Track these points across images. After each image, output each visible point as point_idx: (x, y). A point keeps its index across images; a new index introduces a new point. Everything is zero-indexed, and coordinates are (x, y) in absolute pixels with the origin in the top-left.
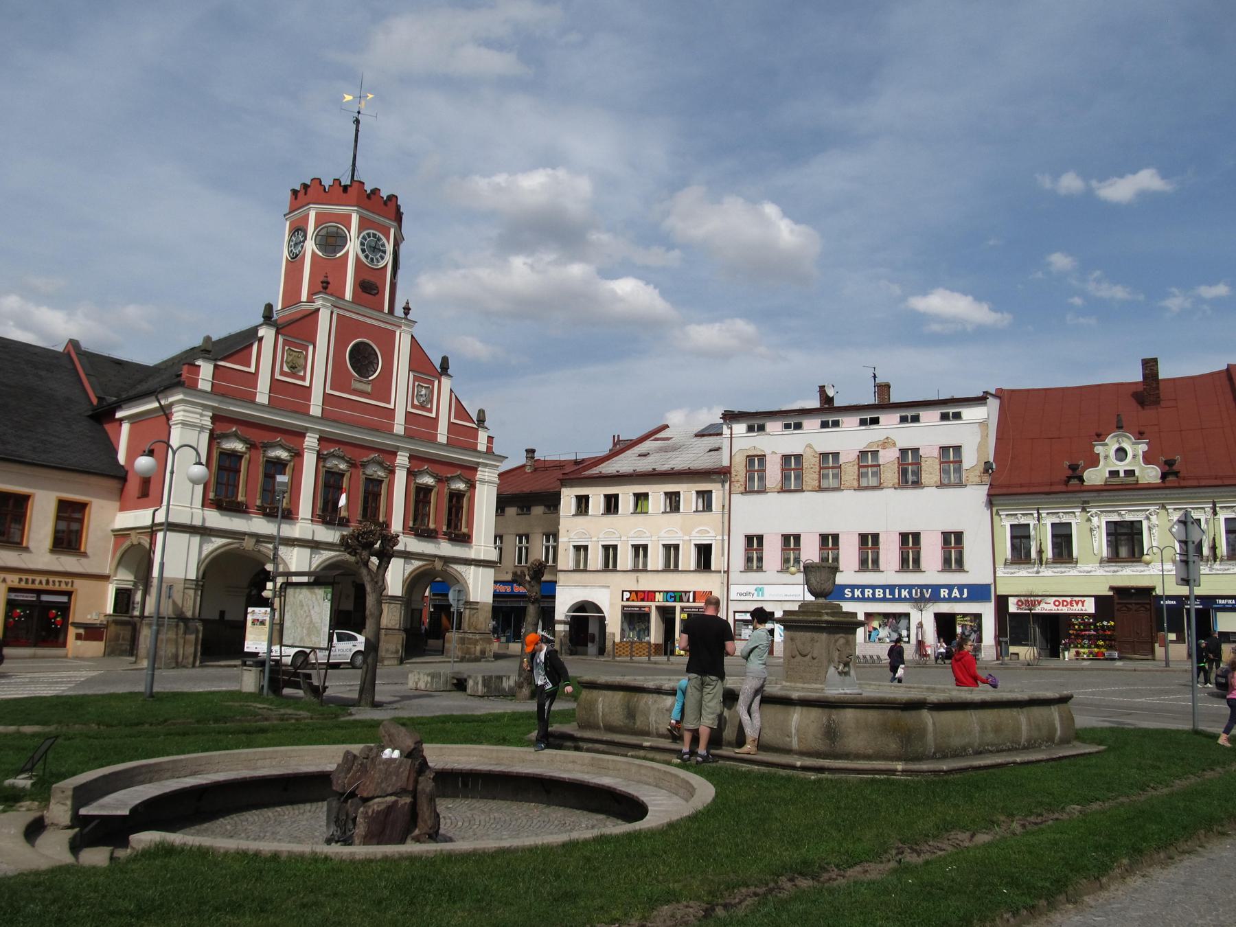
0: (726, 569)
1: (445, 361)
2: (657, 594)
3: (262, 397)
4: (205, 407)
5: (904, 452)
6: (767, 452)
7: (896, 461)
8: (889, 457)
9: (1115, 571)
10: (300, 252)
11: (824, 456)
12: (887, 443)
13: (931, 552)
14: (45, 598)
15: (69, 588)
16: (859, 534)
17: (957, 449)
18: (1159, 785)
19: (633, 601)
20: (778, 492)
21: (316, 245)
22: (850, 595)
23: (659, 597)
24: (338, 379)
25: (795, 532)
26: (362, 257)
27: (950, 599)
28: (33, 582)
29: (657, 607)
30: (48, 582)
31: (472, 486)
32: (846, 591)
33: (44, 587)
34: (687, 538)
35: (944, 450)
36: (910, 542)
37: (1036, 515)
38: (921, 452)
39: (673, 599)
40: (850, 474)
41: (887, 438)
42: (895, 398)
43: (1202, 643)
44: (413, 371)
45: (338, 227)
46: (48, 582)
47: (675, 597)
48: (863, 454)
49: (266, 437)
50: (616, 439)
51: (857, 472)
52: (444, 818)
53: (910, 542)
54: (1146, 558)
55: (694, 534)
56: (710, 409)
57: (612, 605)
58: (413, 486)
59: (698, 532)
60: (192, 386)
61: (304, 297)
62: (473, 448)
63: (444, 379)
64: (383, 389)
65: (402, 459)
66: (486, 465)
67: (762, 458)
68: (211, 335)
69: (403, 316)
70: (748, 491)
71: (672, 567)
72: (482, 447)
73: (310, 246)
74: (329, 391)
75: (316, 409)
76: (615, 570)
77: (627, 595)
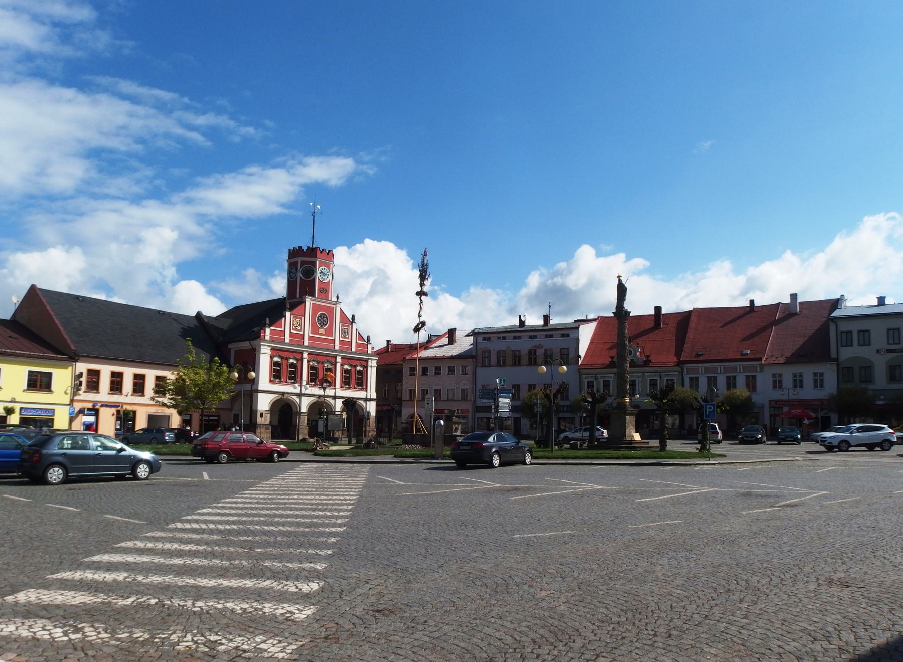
1: (353, 317)
4: (268, 346)
5: (546, 350)
12: (540, 346)
14: (211, 418)
15: (218, 414)
23: (446, 412)
24: (314, 330)
26: (320, 278)
27: (564, 412)
29: (445, 416)
30: (798, 382)
46: (798, 382)
48: (530, 352)
49: (324, 359)
55: (461, 384)
56: (629, 258)
61: (298, 296)
62: (367, 354)
63: (354, 325)
64: (330, 332)
65: (339, 359)
70: (483, 365)
73: (300, 275)
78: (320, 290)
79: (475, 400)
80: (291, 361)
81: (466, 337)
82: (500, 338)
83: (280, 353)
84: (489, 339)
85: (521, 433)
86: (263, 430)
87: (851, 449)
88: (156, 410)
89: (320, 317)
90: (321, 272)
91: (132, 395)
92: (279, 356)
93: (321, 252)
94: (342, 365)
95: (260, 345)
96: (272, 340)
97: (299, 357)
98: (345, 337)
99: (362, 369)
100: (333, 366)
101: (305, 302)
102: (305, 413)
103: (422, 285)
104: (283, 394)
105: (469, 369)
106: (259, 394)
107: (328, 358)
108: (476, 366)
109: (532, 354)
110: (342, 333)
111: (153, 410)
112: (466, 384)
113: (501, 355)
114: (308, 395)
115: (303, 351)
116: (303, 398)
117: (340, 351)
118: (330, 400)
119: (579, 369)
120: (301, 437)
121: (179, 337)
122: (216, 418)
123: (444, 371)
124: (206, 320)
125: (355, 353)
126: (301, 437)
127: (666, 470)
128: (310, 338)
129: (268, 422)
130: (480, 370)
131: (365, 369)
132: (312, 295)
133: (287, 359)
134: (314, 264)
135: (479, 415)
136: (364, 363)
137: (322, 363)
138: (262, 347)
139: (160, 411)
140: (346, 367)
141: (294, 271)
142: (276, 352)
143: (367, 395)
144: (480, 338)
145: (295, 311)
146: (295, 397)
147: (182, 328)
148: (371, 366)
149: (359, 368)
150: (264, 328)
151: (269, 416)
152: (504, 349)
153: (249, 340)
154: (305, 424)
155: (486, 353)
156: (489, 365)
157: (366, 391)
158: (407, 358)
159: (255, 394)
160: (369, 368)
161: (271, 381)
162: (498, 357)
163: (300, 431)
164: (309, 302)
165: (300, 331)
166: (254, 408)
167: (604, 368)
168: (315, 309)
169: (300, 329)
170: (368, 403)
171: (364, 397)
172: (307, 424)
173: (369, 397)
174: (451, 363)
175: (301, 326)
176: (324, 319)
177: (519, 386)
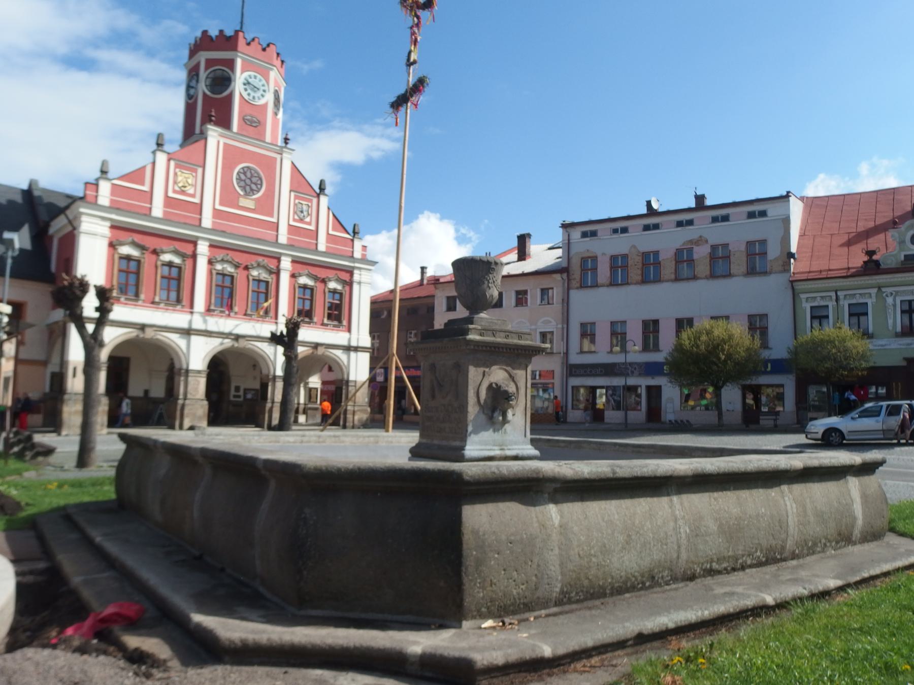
0: (565, 351)
3: (158, 210)
5: (714, 248)
6: (599, 254)
7: (708, 256)
8: (701, 253)
9: (908, 344)
11: (645, 255)
12: (700, 241)
16: (676, 319)
17: (763, 242)
20: (608, 286)
21: (206, 86)
24: (228, 196)
31: (349, 284)
32: (665, 368)
34: (533, 327)
35: (750, 244)
36: (651, 328)
37: (834, 298)
38: (730, 248)
40: (668, 270)
41: (701, 237)
42: (709, 202)
43: (882, 389)
45: (223, 70)
48: (679, 252)
49: (252, 260)
51: (674, 267)
52: (359, 283)
55: (539, 324)
58: (116, 257)
59: (542, 322)
60: (94, 204)
64: (267, 205)
65: (286, 264)
66: (360, 269)
67: (594, 259)
68: (493, 434)
69: (284, 145)
70: (583, 286)
74: (218, 207)
75: (207, 221)
78: (243, 119)
79: (567, 354)
82: (615, 231)
83: (138, 238)
84: (594, 234)
85: (663, 419)
87: (313, 345)
90: (247, 83)
92: (310, 276)
94: (293, 276)
96: (115, 207)
98: (301, 220)
100: (274, 276)
102: (199, 372)
104: (143, 327)
105: (556, 294)
107: (260, 259)
108: (568, 289)
109: (684, 258)
110: (295, 213)
112: (549, 320)
113: (618, 263)
116: (194, 338)
117: (290, 246)
118: (339, 353)
119: (792, 282)
128: (217, 214)
130: (578, 297)
132: (224, 122)
134: (231, 64)
135: (574, 381)
136: (345, 277)
137: (246, 268)
140: (303, 280)
143: (349, 340)
144: (576, 234)
148: (359, 283)
149: (332, 285)
152: (625, 251)
155: (589, 264)
156: (595, 285)
157: (349, 330)
160: (356, 287)
162: (613, 268)
163: (186, 411)
165: (193, 196)
166: (65, 359)
167: (853, 276)
168: (230, 156)
170: (353, 354)
171: (345, 343)
173: (354, 344)
175: (195, 186)
176: (254, 180)
177: (656, 322)
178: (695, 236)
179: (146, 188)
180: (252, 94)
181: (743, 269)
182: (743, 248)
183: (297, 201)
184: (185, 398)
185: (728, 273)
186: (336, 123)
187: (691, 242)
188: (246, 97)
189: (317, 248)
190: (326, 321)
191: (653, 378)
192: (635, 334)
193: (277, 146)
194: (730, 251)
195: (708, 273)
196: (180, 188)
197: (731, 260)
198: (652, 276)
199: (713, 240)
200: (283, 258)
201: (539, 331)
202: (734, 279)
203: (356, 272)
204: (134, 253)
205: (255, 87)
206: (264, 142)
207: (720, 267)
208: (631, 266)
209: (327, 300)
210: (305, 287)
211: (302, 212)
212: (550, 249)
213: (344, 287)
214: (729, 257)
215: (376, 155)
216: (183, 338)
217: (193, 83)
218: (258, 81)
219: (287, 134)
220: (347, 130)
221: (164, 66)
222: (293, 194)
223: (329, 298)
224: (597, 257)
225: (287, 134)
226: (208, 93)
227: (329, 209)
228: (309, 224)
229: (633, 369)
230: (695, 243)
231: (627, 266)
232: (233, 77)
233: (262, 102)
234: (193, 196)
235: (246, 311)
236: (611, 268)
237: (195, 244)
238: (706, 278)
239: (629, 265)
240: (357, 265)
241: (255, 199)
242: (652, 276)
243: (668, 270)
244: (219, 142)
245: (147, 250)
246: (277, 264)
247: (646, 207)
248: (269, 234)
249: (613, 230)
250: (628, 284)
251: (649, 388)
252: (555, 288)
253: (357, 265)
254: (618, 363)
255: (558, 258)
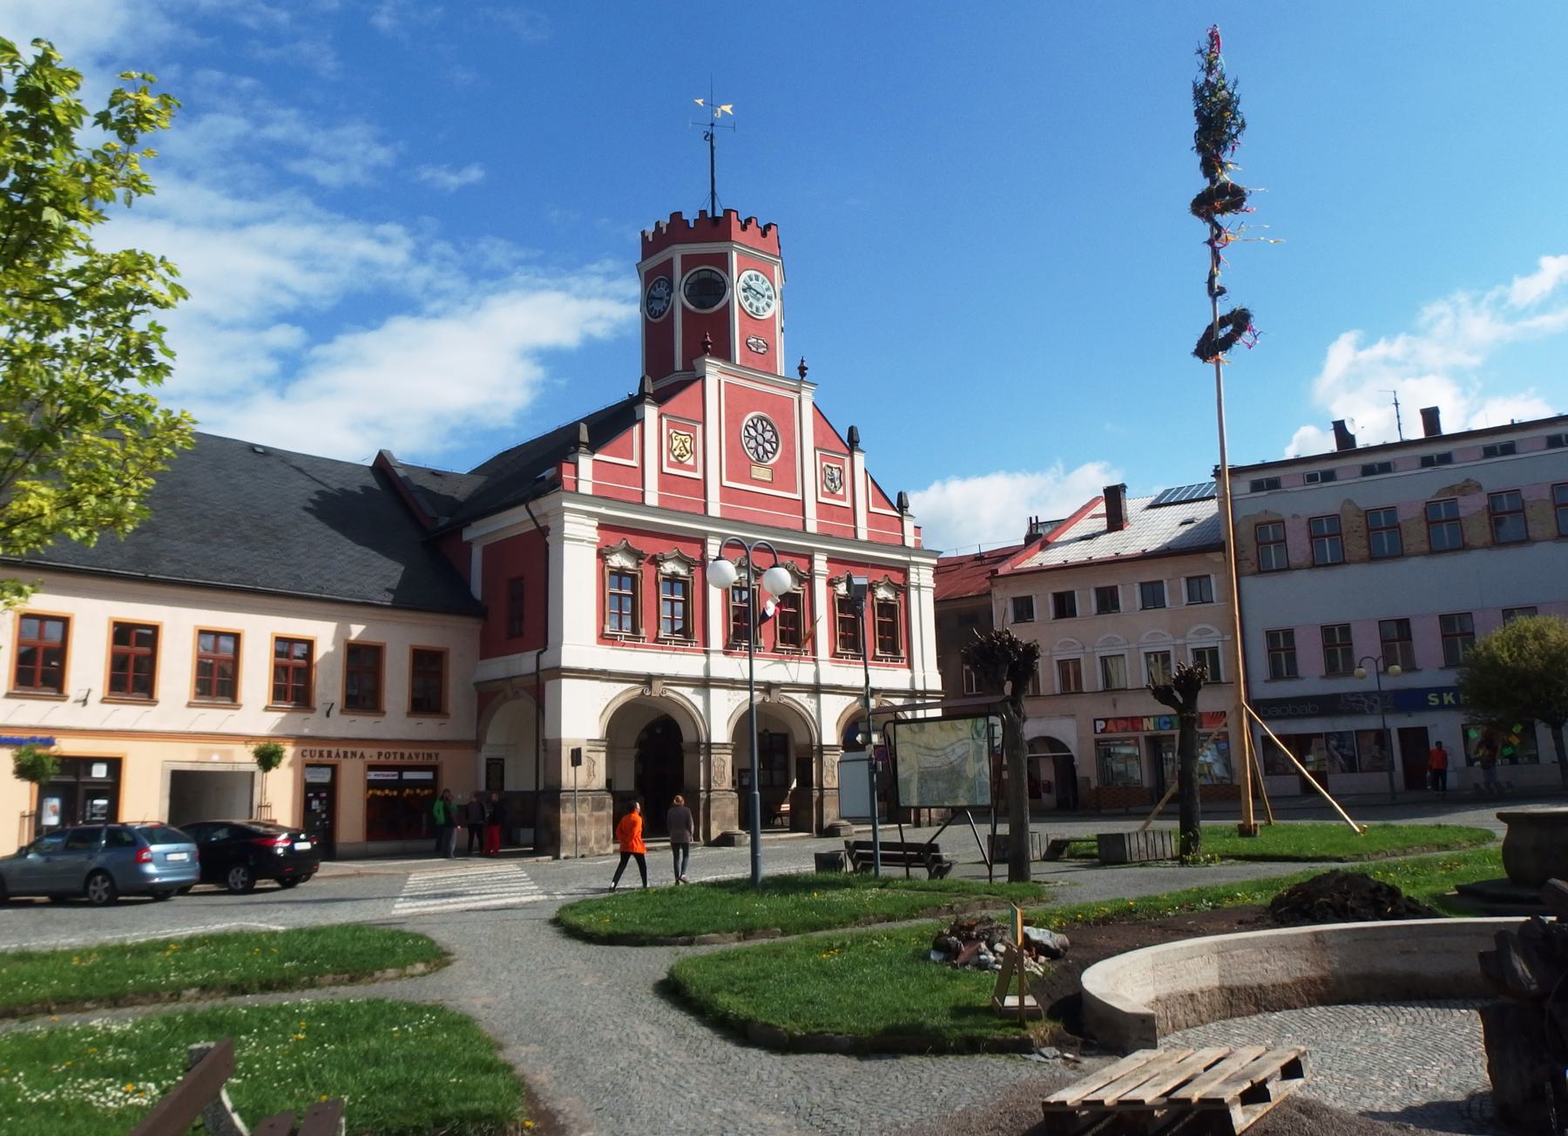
2: (1145, 720)
4: (590, 514)
5: (1494, 497)
6: (1286, 515)
7: (1485, 511)
8: (1472, 506)
10: (665, 309)
11: (1370, 515)
12: (1468, 487)
13: (1310, 655)
14: (407, 775)
15: (433, 761)
16: (1322, 627)
18: (642, 1016)
19: (1111, 732)
20: (1309, 568)
22: (1437, 701)
24: (738, 464)
25: (1285, 625)
26: (746, 305)
28: (321, 754)
29: (1146, 738)
32: (1430, 697)
33: (406, 761)
36: (1337, 640)
38: (1524, 495)
39: (1168, 726)
44: (820, 449)
47: (1171, 723)
48: (1430, 506)
50: (1034, 521)
51: (1425, 531)
53: (1337, 640)
54: (1357, 671)
55: (1190, 635)
57: (1080, 740)
61: (679, 365)
64: (787, 474)
66: (917, 564)
71: (1073, 689)
72: (910, 542)
73: (680, 299)
76: (1079, 691)
77: (1101, 725)
80: (669, 567)
81: (1152, 511)
82: (1312, 478)
84: (1274, 484)
86: (584, 812)
88: (201, 751)
89: (755, 427)
90: (748, 288)
91: (103, 701)
92: (629, 551)
93: (744, 228)
95: (561, 511)
96: (599, 497)
97: (693, 552)
98: (832, 494)
99: (891, 596)
100: (805, 586)
101: (703, 378)
102: (724, 746)
103: (1211, 165)
104: (648, 680)
106: (564, 681)
110: (824, 482)
111: (188, 756)
113: (1324, 531)
114: (730, 684)
115: (707, 534)
118: (803, 699)
120: (715, 833)
121: (305, 514)
122: (428, 775)
123: (1130, 597)
124: (401, 473)
125: (868, 544)
126: (715, 833)
127: (1328, 827)
128: (726, 492)
129: (600, 781)
131: (902, 597)
132: (724, 353)
133: (656, 561)
134: (723, 261)
136: (897, 578)
138: (567, 517)
139: (215, 758)
141: (662, 290)
142: (616, 539)
143: (913, 680)
144: (1244, 486)
145: (673, 405)
146: (687, 692)
147: (318, 493)
148: (918, 587)
150: (570, 458)
151: (601, 759)
152: (1336, 510)
153: (523, 501)
154: (727, 783)
156: (1287, 568)
157: (910, 666)
158: (1001, 572)
159: (549, 685)
160: (913, 594)
161: (604, 638)
164: (714, 374)
165: (693, 469)
166: (549, 735)
168: (736, 401)
169: (690, 462)
172: (734, 783)
173: (919, 686)
174: (1149, 574)
178: (1458, 480)
179: (635, 463)
180: (755, 304)
181: (1551, 529)
182: (1547, 495)
183: (824, 464)
184: (709, 790)
185: (1525, 537)
186: (519, 277)
187: (1451, 489)
188: (748, 310)
189: (856, 537)
190: (779, 646)
191: (1410, 716)
192: (1367, 644)
193: (776, 376)
194: (1523, 501)
195: (1488, 538)
196: (676, 457)
197: (1528, 516)
198: (1386, 547)
199: (1491, 485)
200: (817, 556)
201: (1189, 647)
202: (1537, 546)
203: (913, 570)
204: (628, 563)
205: (758, 293)
206: (776, 375)
207: (1510, 527)
208: (1348, 533)
209: (732, 604)
210: (620, 573)
211: (832, 480)
212: (1152, 507)
213: (896, 595)
214: (1522, 511)
215: (599, 330)
216: (699, 694)
217: (662, 290)
218: (761, 285)
219: (802, 361)
220: (543, 288)
221: (210, 196)
222: (818, 453)
223: (610, 587)
224: (1283, 522)
225: (802, 361)
226: (692, 307)
227: (866, 471)
228: (843, 498)
229: (1372, 703)
230: (1459, 490)
231: (1340, 534)
232: (728, 280)
233: (767, 315)
234: (693, 469)
235: (775, 644)
236: (1312, 538)
237: (703, 543)
238: (1486, 546)
239: (1344, 532)
240: (914, 559)
241: (771, 465)
242: (1386, 547)
243: (1415, 536)
244: (719, 381)
245: (643, 559)
246: (808, 566)
247: (1381, 443)
248: (793, 520)
249: (1308, 476)
250: (1344, 563)
251: (1403, 732)
252: (1212, 576)
253: (914, 559)
254: (1344, 694)
255: (1182, 524)
